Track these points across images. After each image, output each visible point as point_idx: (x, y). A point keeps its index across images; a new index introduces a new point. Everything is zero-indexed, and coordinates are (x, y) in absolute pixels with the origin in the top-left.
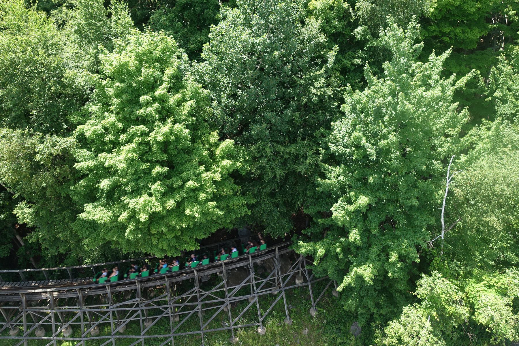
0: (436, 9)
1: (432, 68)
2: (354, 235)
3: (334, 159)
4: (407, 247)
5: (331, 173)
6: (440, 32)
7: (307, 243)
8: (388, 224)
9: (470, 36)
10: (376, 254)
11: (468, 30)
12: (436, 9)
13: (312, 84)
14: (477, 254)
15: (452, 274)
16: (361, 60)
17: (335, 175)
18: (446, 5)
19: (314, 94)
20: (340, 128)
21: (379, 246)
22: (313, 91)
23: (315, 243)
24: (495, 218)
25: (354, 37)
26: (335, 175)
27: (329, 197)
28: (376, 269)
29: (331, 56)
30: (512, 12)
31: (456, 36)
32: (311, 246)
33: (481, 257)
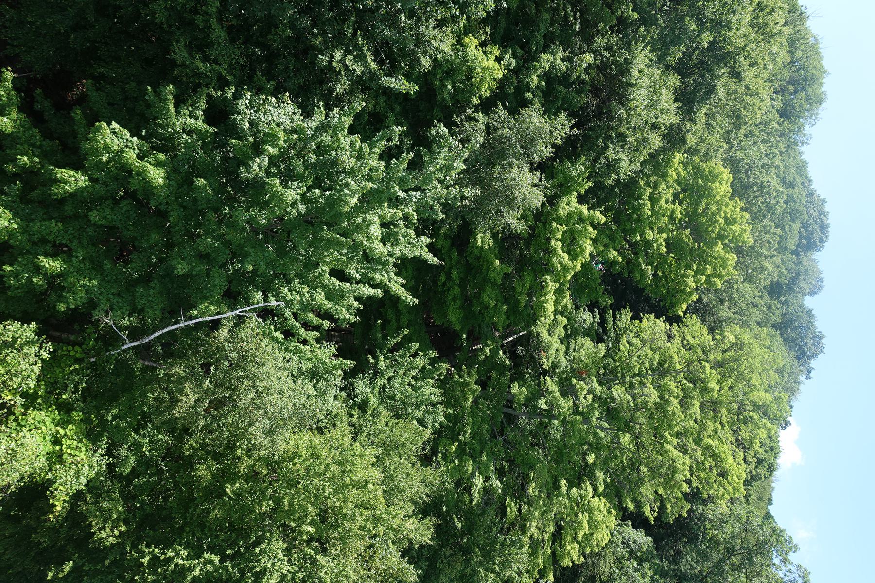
0: (482, 247)
1: (409, 243)
2: (73, 180)
3: (219, 114)
4: (84, 286)
5: (190, 116)
6: (451, 268)
7: (15, 88)
8: (115, 246)
9: (451, 308)
10: (44, 233)
11: (459, 303)
12: (482, 247)
13: (348, 52)
14: (115, 411)
15: (56, 383)
16: (398, 143)
17: (187, 122)
18: (488, 262)
19: (332, 57)
20: (281, 114)
21: (66, 237)
22: (338, 55)
23: (21, 110)
24: (193, 400)
25: (430, 125)
26: (187, 122)
27: (139, 120)
28: (10, 239)
29: (399, 84)
30: (487, 350)
31: (449, 290)
32: (9, 99)
33: (110, 418)
